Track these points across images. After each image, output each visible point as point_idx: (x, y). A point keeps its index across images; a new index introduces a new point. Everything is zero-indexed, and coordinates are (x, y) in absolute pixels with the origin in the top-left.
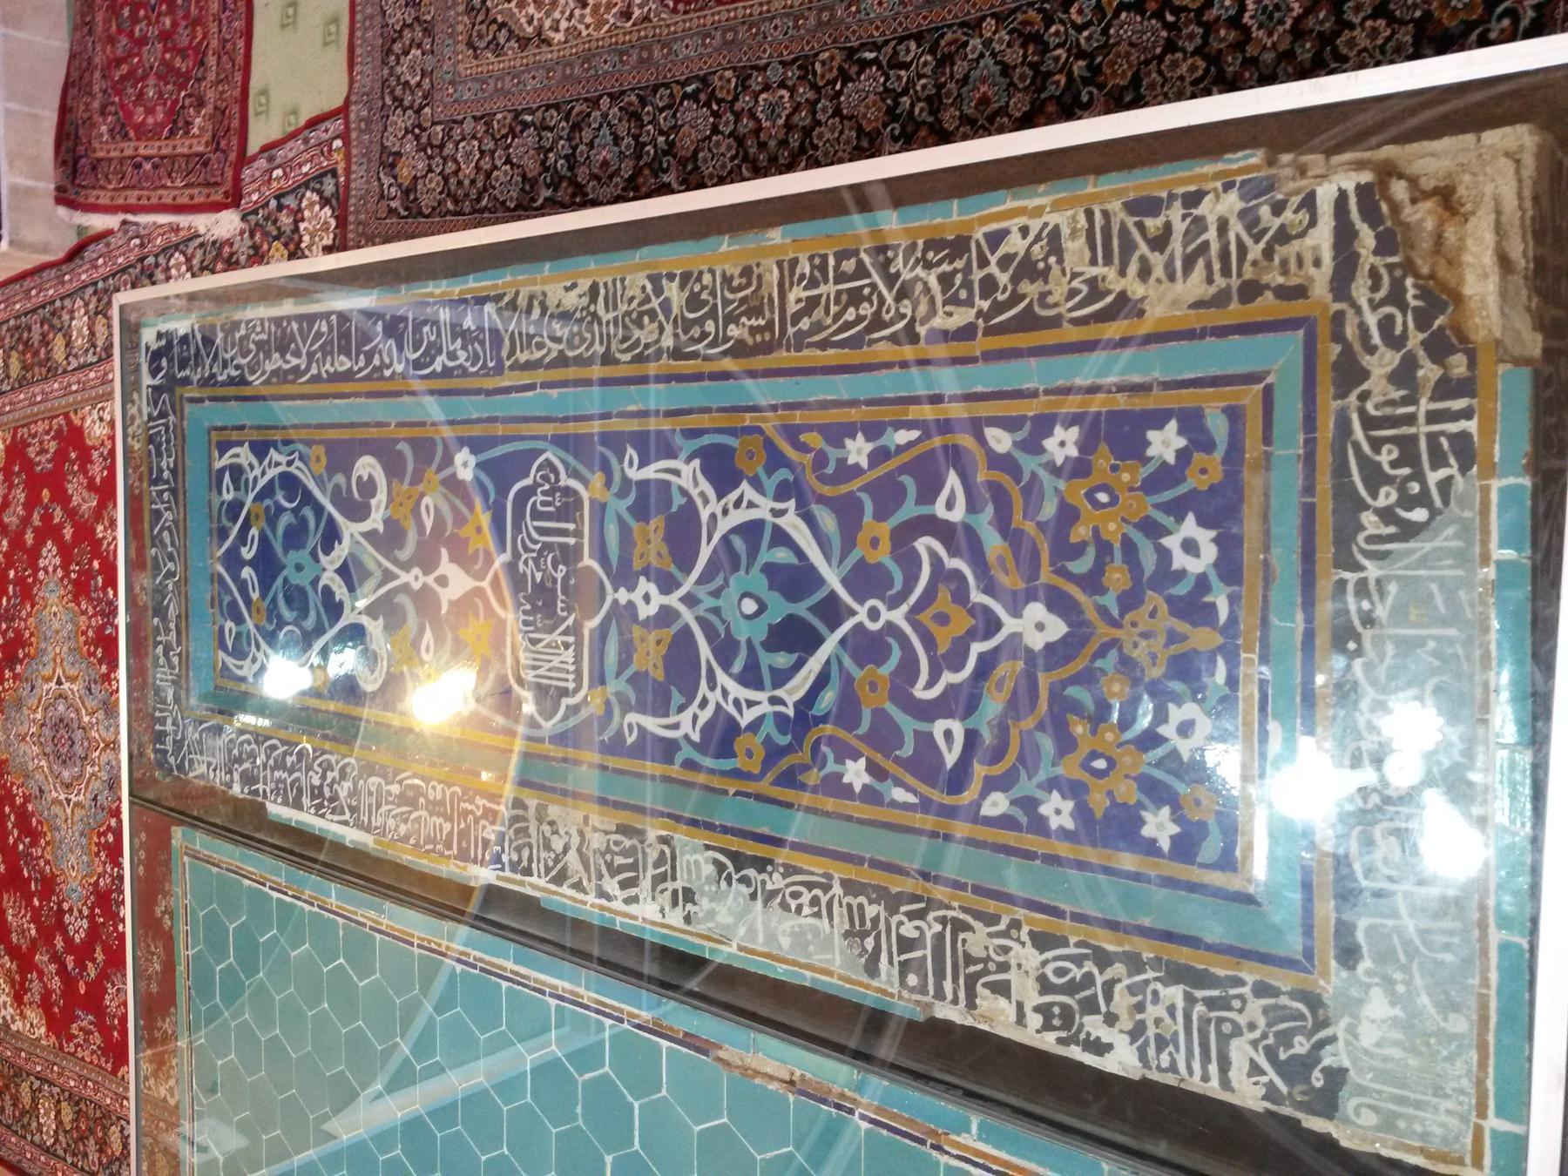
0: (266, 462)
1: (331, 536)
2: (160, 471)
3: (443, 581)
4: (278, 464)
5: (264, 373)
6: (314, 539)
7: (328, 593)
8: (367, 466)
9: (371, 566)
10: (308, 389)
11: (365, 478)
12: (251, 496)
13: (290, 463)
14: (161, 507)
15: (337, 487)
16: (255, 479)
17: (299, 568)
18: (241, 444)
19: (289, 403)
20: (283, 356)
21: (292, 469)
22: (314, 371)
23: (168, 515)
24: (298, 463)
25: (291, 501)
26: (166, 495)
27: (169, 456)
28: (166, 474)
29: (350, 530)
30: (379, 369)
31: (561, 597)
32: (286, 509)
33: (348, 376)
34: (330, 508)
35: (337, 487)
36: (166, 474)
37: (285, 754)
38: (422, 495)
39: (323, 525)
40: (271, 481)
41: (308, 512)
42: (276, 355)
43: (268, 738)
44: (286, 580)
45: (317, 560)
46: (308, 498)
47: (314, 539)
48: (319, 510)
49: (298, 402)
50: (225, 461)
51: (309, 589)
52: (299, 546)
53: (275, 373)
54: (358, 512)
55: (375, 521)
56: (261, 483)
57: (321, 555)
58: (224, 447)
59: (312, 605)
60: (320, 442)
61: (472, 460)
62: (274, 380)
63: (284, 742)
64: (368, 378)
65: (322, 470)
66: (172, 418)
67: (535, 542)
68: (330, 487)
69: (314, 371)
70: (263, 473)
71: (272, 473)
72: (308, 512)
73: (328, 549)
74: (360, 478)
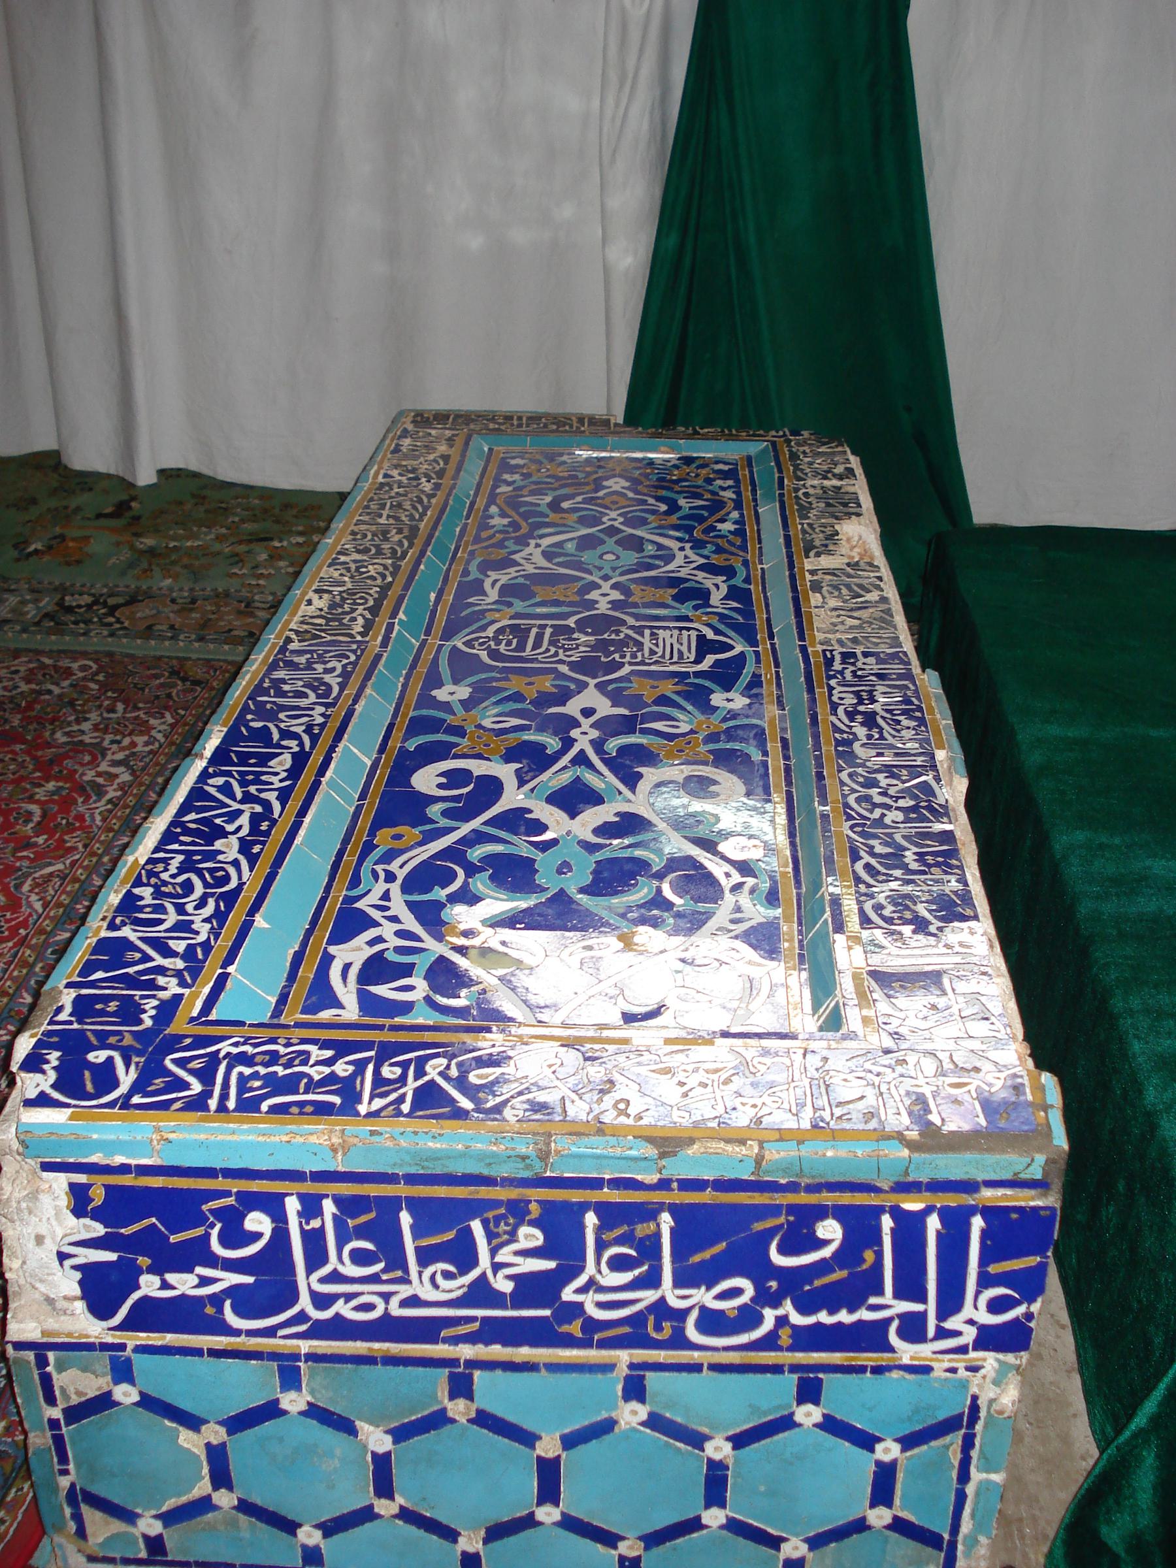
0: (376, 915)
1: (517, 820)
2: (332, 1078)
3: (588, 712)
4: (386, 896)
5: (236, 863)
6: (521, 846)
7: (604, 830)
8: (426, 780)
9: (566, 778)
10: (294, 804)
11: (443, 780)
12: (429, 943)
13: (390, 877)
14: (412, 1085)
15: (445, 813)
16: (401, 934)
17: (564, 868)
18: (328, 959)
19: (302, 832)
20: (224, 834)
21: (401, 875)
22: (272, 796)
23: (433, 1070)
24: (394, 867)
25: (453, 876)
26: (388, 1072)
27: (305, 1058)
28: (342, 1068)
29: (513, 797)
30: (309, 729)
31: (606, 636)
32: (466, 884)
33: (300, 759)
34: (476, 823)
35: (445, 813)
36: (342, 1068)
37: (872, 854)
38: (479, 726)
39: (502, 834)
40: (411, 905)
41: (476, 854)
42: (219, 844)
43: (858, 880)
44: (582, 890)
45: (554, 842)
46: (454, 854)
47: (521, 846)
48: (478, 838)
49: (307, 820)
50: (347, 994)
51: (599, 856)
52: (528, 865)
53: (245, 847)
54: (491, 788)
55: (506, 772)
56: (410, 923)
57: (548, 836)
58: (322, 994)
59: (627, 853)
60: (372, 833)
61: (448, 687)
62: (256, 849)
63: (855, 857)
64: (314, 739)
65: (416, 831)
66: (225, 1047)
67: (548, 650)
68: (444, 822)
69: (272, 796)
70: (394, 919)
71: (398, 905)
72: (476, 854)
73: (539, 827)
74: (440, 786)
